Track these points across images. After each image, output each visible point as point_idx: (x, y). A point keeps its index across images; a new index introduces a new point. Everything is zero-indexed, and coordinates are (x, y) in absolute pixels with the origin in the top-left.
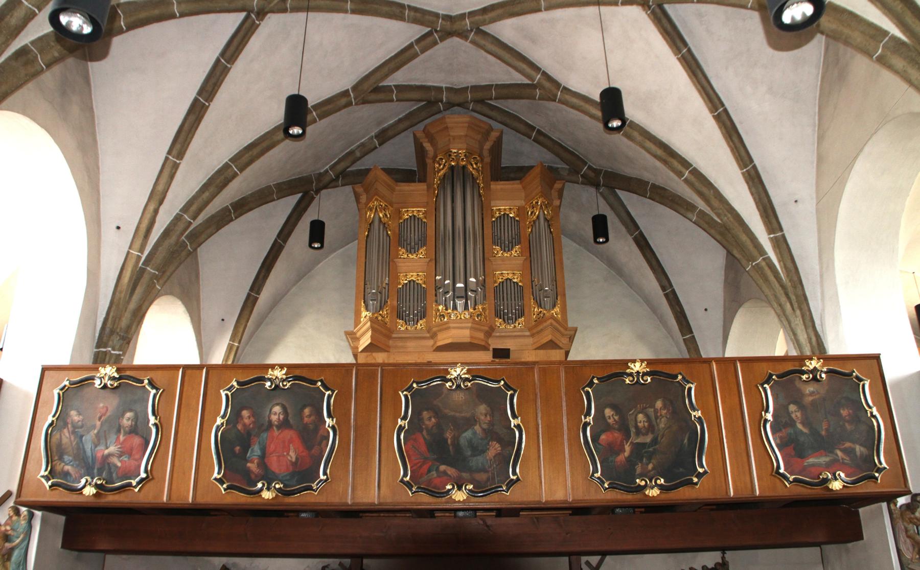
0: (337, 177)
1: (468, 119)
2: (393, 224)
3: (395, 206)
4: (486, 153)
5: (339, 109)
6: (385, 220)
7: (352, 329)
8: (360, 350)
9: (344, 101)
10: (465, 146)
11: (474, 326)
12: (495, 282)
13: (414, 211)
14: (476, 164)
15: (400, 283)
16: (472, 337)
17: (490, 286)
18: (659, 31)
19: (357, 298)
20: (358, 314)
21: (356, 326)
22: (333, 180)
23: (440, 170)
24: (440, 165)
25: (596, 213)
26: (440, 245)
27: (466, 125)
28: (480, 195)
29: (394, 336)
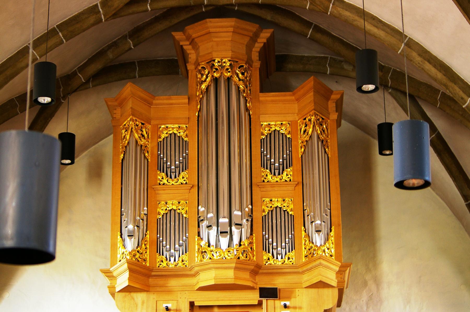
0: (87, 82)
1: (233, 24)
2: (151, 146)
3: (153, 122)
4: (255, 56)
5: (88, 28)
6: (142, 142)
7: (108, 267)
8: (117, 290)
9: (92, 19)
10: (230, 54)
11: (239, 266)
12: (264, 211)
13: (173, 128)
14: (243, 74)
15: (159, 214)
16: (236, 278)
17: (258, 216)
18: (239, 291)
19: (112, 230)
20: (114, 247)
21: (111, 267)
22: (83, 84)
23: (202, 82)
24: (202, 75)
25: (382, 121)
26: (204, 168)
27: (231, 29)
28: (247, 110)
29: (153, 273)
